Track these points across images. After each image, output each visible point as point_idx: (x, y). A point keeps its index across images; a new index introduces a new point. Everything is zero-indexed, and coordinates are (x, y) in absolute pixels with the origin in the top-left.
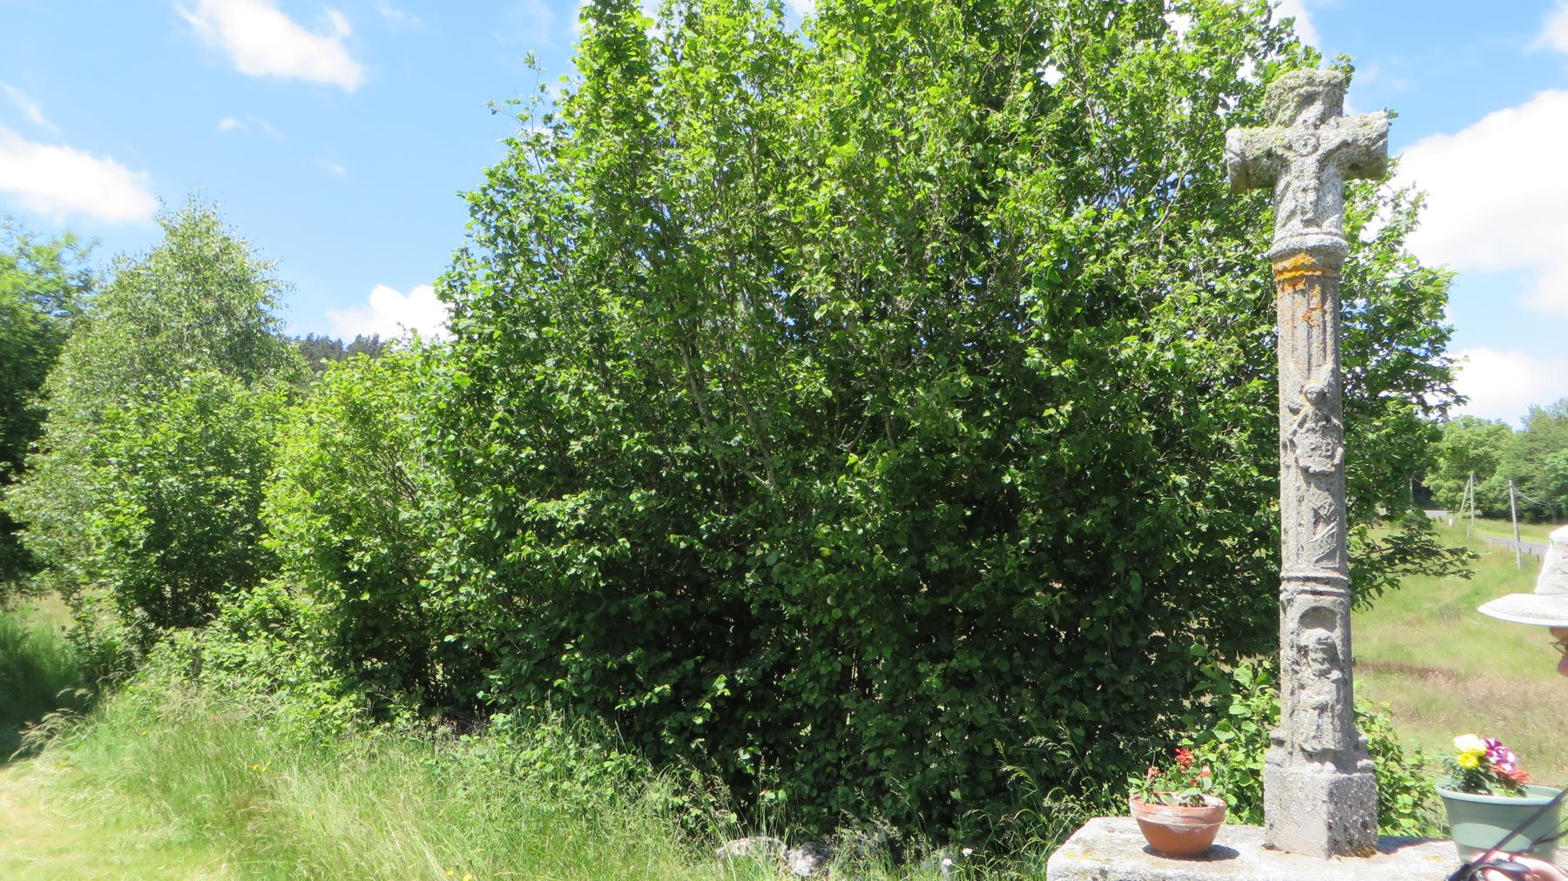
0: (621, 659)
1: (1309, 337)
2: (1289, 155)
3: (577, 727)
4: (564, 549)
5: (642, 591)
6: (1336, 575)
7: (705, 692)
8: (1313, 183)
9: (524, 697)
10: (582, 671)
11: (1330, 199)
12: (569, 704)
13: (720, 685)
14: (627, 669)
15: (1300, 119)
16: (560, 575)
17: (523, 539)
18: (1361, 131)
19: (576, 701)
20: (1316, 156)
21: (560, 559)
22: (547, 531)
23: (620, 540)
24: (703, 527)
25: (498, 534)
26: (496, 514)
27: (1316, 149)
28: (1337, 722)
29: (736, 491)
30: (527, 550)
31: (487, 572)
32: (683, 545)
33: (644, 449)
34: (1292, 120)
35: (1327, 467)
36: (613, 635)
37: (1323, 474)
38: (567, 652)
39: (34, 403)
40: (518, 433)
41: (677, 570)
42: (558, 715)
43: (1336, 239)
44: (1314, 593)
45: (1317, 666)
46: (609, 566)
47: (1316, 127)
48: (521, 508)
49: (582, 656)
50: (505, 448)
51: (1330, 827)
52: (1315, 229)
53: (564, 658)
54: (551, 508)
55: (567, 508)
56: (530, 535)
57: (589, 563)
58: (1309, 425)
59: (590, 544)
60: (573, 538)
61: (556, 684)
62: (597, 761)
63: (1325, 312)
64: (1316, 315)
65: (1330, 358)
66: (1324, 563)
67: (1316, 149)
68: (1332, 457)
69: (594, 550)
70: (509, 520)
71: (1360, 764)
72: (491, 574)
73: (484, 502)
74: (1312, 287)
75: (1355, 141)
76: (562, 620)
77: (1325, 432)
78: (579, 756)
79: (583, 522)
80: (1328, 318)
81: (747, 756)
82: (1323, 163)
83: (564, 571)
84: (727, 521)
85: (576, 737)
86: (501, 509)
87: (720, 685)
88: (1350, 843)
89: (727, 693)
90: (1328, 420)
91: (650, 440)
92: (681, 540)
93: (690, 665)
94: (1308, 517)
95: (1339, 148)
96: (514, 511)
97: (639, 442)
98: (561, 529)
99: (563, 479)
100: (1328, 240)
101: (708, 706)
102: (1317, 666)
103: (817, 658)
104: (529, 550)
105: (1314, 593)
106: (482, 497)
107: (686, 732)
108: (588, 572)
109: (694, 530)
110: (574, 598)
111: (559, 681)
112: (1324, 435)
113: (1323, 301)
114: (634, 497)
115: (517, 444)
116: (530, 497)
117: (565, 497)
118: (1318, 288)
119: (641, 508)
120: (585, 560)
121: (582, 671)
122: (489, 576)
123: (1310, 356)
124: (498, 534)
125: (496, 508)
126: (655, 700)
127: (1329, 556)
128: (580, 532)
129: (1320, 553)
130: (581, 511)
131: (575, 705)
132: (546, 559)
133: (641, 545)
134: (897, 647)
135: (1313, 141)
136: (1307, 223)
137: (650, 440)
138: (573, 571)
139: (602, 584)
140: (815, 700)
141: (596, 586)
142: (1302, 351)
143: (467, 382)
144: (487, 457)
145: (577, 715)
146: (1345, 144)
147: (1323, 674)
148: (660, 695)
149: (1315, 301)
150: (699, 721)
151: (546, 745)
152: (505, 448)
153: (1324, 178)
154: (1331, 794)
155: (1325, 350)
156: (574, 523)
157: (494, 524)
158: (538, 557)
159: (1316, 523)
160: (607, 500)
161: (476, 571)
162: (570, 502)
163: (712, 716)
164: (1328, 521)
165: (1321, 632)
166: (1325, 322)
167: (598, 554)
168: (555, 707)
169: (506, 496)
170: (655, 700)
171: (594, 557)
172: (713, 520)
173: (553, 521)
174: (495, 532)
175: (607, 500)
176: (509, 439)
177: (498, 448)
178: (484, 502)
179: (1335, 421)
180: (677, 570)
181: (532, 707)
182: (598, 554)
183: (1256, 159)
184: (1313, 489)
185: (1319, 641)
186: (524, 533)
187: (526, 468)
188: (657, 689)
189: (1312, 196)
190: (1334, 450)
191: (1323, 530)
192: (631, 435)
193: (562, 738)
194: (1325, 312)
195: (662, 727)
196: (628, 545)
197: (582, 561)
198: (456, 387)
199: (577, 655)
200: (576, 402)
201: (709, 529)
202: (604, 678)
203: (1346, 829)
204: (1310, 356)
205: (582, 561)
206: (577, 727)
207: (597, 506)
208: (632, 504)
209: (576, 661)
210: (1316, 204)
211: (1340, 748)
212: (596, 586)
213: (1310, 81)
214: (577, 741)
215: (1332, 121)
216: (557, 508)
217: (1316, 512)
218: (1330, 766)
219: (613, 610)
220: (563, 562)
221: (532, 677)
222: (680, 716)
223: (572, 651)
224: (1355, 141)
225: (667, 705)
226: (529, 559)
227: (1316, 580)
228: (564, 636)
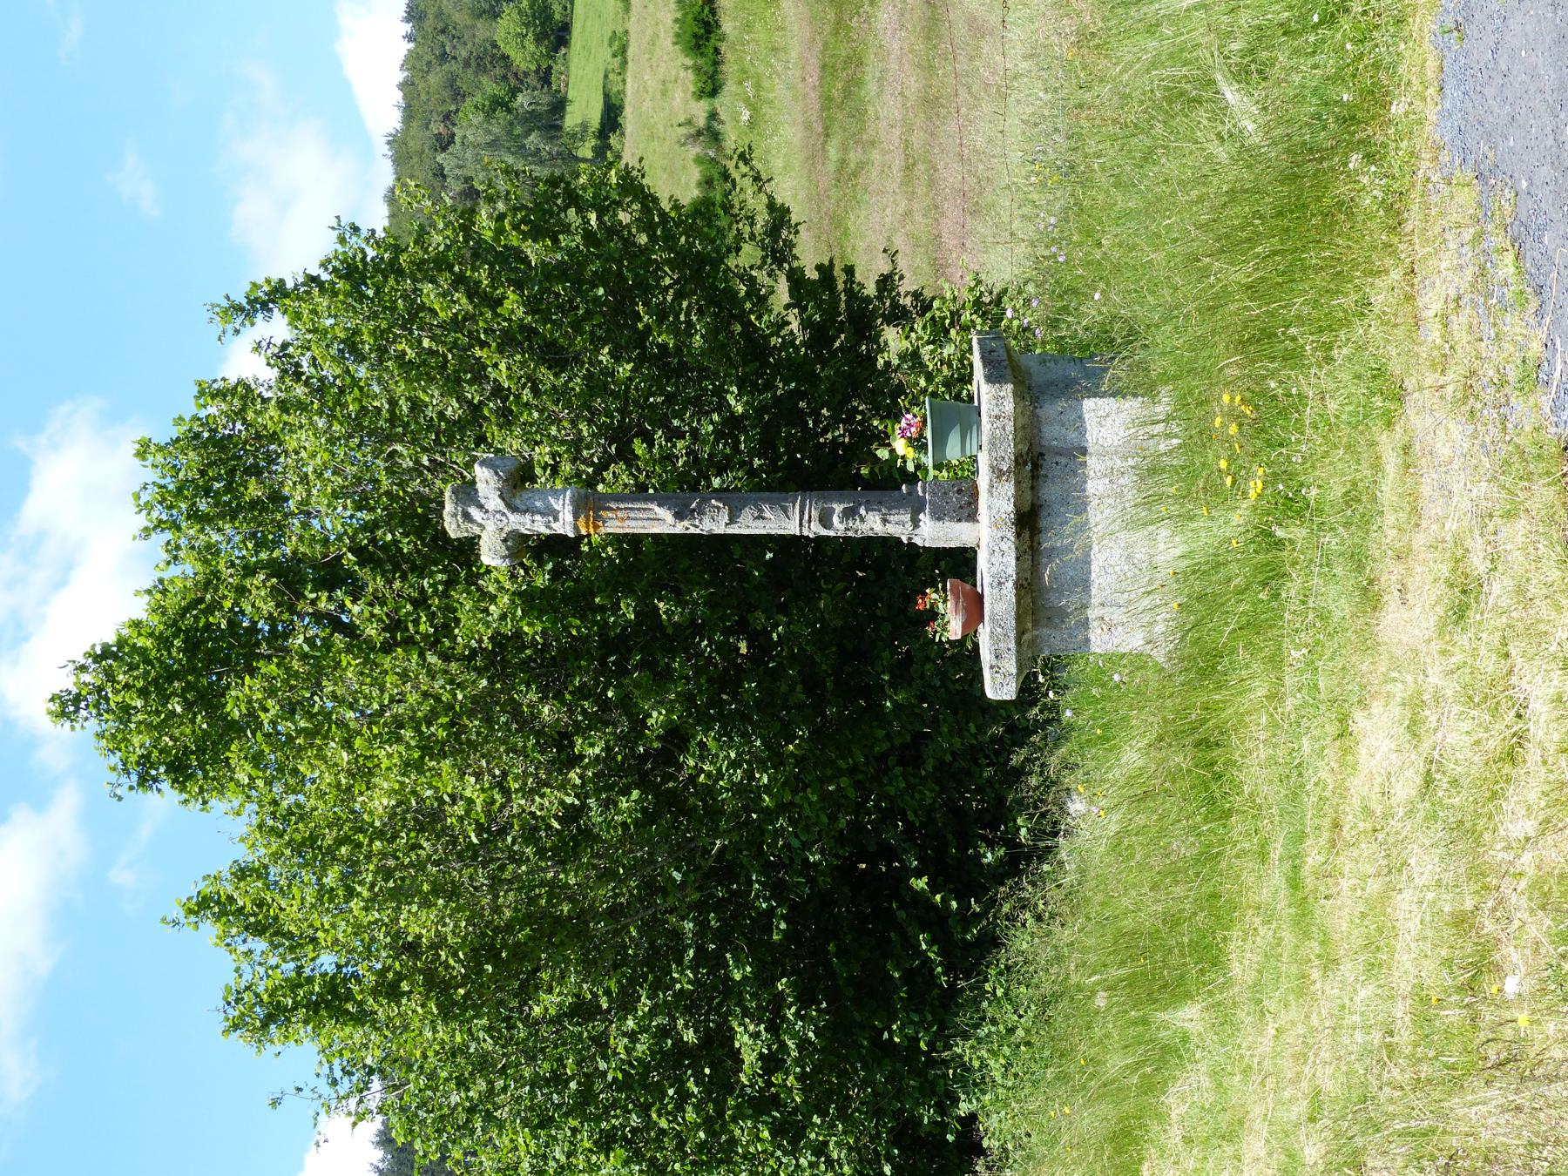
0: (898, 983)
1: (636, 519)
2: (507, 529)
3: (967, 1025)
4: (790, 1043)
5: (828, 964)
6: (797, 506)
7: (929, 899)
8: (528, 516)
9: (942, 1082)
10: (912, 1022)
11: (538, 504)
12: (945, 1035)
13: (921, 884)
14: (908, 976)
15: (480, 521)
16: (815, 1048)
17: (779, 1085)
18: (492, 484)
19: (942, 1027)
20: (509, 514)
21: (800, 1047)
22: (772, 1063)
23: (780, 988)
24: (764, 905)
25: (776, 1114)
26: (755, 1118)
27: (504, 514)
28: (893, 512)
29: (726, 870)
30: (791, 1081)
31: (815, 1124)
32: (783, 926)
33: (689, 967)
34: (480, 525)
35: (726, 511)
36: (874, 994)
37: (730, 515)
38: (891, 1038)
39: (862, 511)
40: (672, 1097)
41: (808, 929)
42: (957, 1045)
43: (567, 501)
44: (810, 521)
45: (858, 523)
46: (806, 999)
47: (487, 511)
48: (749, 1090)
49: (895, 1022)
50: (689, 1108)
51: (959, 520)
52: (561, 515)
53: (897, 1040)
54: (749, 1058)
55: (748, 1044)
56: (777, 1079)
57: (802, 1018)
58: (697, 523)
59: (784, 1019)
60: (778, 1036)
61: (925, 1048)
62: (999, 1003)
63: (618, 509)
64: (620, 514)
65: (651, 506)
66: (790, 514)
67: (504, 514)
68: (718, 508)
69: (790, 1013)
70: (761, 1104)
71: (921, 494)
72: (816, 1120)
73: (742, 1129)
74: (601, 516)
75: (499, 489)
76: (862, 1046)
77: (701, 513)
78: (994, 1022)
79: (763, 1026)
80: (622, 506)
81: (989, 855)
82: (514, 509)
83: (811, 1043)
84: (758, 881)
85: (977, 1026)
86: (750, 1112)
87: (921, 884)
88: (970, 504)
89: (925, 879)
90: (694, 510)
91: (680, 962)
92: (778, 927)
93: (902, 914)
94: (760, 523)
95: (503, 499)
96: (752, 1098)
97: (682, 973)
98: (769, 1049)
99: (718, 1046)
100: (569, 508)
101: (938, 897)
102: (858, 523)
103: (891, 790)
104: (791, 1078)
105: (810, 521)
106: (737, 1132)
107: (967, 920)
108: (812, 1018)
109: (770, 912)
110: (838, 1033)
111: (922, 1044)
112: (704, 514)
113: (611, 509)
114: (737, 976)
115: (683, 1096)
116: (738, 1081)
117: (737, 1045)
118: (602, 513)
119: (749, 969)
120: (801, 1023)
121: (912, 1022)
122: (819, 1121)
123: (649, 519)
124: (776, 1114)
125: (749, 1117)
126: (935, 948)
127: (785, 510)
128: (773, 1028)
129: (783, 516)
130: (751, 1028)
131: (948, 1029)
132: (797, 1062)
133: (784, 966)
134: (875, 724)
135: (498, 516)
136: (556, 519)
137: (680, 962)
138: (811, 1034)
139: (824, 1005)
140: (931, 791)
141: (826, 1011)
142: (646, 523)
143: (619, 1153)
144: (698, 1127)
145: (956, 1026)
146: (501, 496)
147: (862, 520)
148: (930, 943)
149: (610, 515)
150: (954, 904)
151: (986, 1056)
152: (689, 1108)
153: (524, 508)
154: (939, 519)
155: (645, 509)
156: (764, 1035)
157: (766, 1118)
158: (798, 1070)
159: (763, 518)
160: (740, 1003)
161: (813, 1136)
162: (742, 1040)
163: (950, 891)
164: (761, 511)
165: (835, 519)
166: (626, 509)
167: (793, 1010)
168: (948, 1047)
169: (738, 1107)
170: (935, 948)
171: (797, 1014)
172: (757, 897)
173: (761, 1057)
174: (773, 1117)
175: (740, 1003)
176: (680, 1108)
177: (691, 1115)
178: (741, 1131)
179: (694, 505)
180: (808, 929)
181: (951, 1071)
182: (793, 1010)
183: (508, 548)
184: (740, 520)
185: (841, 522)
186: (774, 1085)
187: (708, 1086)
188: (924, 947)
189: (538, 517)
190: (714, 506)
191: (767, 514)
192: (675, 981)
193: (979, 1040)
194: (618, 509)
195: (964, 940)
196: (784, 980)
197: (801, 1027)
198: (626, 1163)
199: (895, 1027)
200: (644, 1037)
201: (766, 900)
202: (916, 1002)
203: (961, 507)
204: (649, 519)
205: (801, 1027)
206: (967, 1025)
207: (746, 1012)
208: (744, 978)
209: (901, 1029)
210: (543, 514)
211: (909, 510)
212: (826, 1011)
213: (454, 515)
214: (981, 1024)
215: (483, 501)
216: (750, 1051)
217: (758, 518)
218: (921, 516)
219: (849, 992)
220: (803, 1044)
221: (920, 1074)
222: (951, 921)
223: (891, 1032)
224: (499, 489)
225: (942, 938)
226: (800, 1078)
227: (801, 520)
228: (876, 1040)
